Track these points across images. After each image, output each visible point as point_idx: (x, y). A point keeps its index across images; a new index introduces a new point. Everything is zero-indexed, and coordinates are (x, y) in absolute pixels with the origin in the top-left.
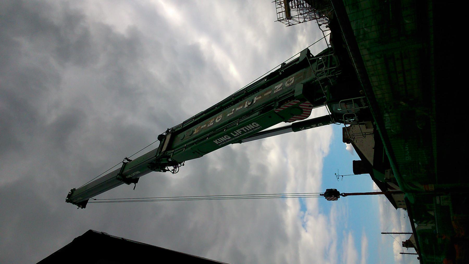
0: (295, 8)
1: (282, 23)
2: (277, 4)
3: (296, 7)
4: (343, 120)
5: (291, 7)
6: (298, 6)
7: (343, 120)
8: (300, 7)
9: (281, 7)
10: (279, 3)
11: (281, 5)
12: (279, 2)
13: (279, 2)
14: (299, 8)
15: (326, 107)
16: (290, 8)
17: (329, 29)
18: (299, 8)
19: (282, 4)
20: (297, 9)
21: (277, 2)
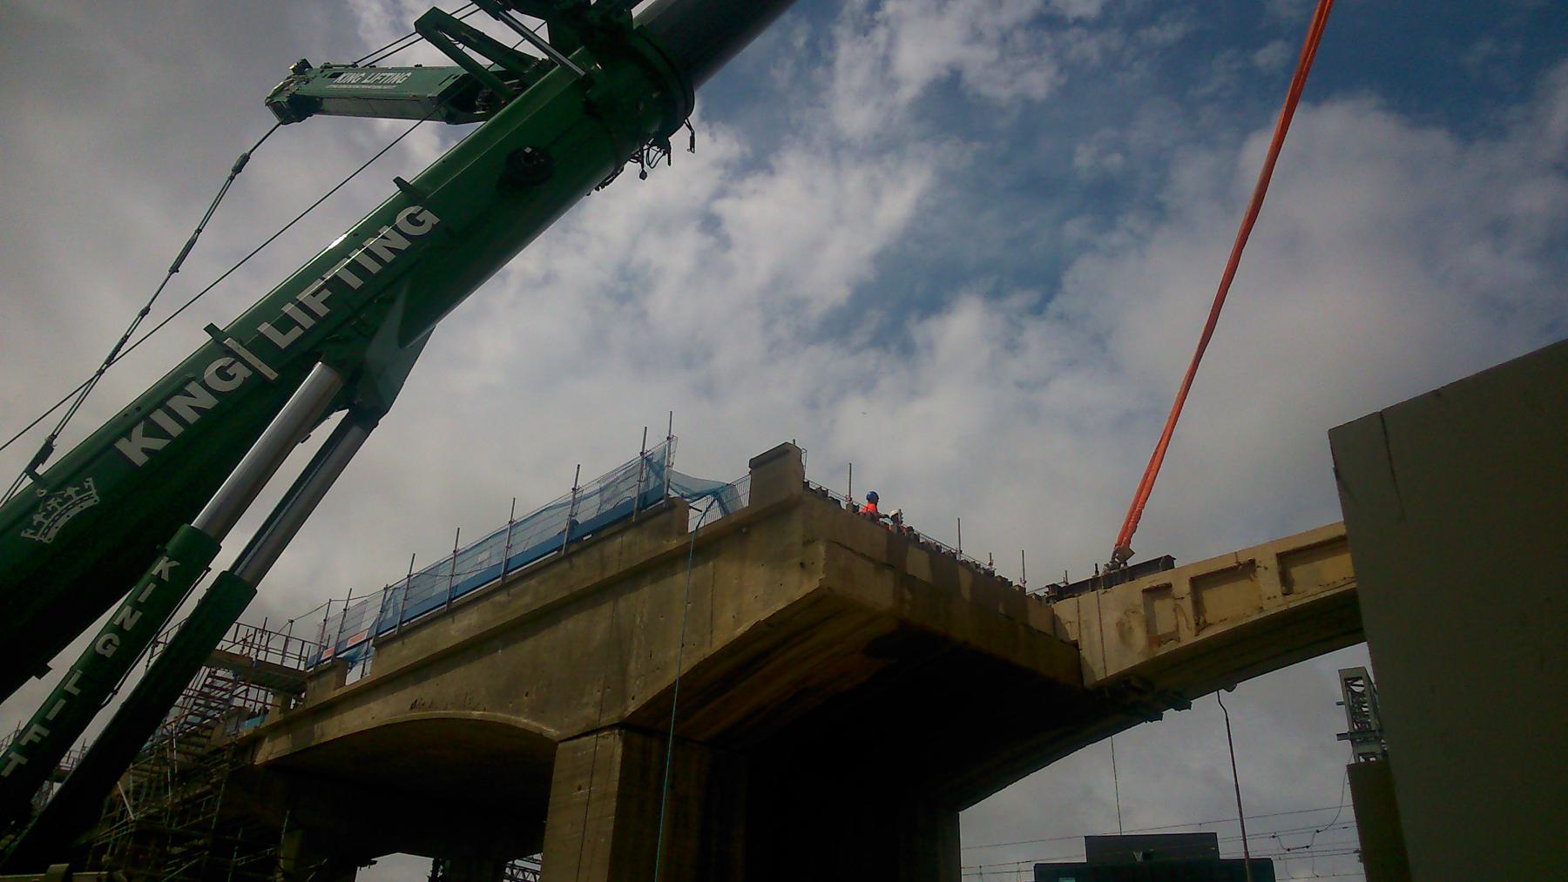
0: (204, 685)
1: (9, 736)
2: (252, 631)
3: (206, 690)
4: (235, 856)
5: (215, 672)
6: (207, 696)
7: (235, 856)
8: (199, 701)
9: (234, 642)
10: (250, 640)
11: (242, 643)
12: (253, 640)
13: (253, 640)
14: (197, 698)
15: (496, 578)
16: (213, 669)
17: (478, 8)
18: (197, 698)
19: (243, 648)
20: (189, 707)
21: (258, 635)
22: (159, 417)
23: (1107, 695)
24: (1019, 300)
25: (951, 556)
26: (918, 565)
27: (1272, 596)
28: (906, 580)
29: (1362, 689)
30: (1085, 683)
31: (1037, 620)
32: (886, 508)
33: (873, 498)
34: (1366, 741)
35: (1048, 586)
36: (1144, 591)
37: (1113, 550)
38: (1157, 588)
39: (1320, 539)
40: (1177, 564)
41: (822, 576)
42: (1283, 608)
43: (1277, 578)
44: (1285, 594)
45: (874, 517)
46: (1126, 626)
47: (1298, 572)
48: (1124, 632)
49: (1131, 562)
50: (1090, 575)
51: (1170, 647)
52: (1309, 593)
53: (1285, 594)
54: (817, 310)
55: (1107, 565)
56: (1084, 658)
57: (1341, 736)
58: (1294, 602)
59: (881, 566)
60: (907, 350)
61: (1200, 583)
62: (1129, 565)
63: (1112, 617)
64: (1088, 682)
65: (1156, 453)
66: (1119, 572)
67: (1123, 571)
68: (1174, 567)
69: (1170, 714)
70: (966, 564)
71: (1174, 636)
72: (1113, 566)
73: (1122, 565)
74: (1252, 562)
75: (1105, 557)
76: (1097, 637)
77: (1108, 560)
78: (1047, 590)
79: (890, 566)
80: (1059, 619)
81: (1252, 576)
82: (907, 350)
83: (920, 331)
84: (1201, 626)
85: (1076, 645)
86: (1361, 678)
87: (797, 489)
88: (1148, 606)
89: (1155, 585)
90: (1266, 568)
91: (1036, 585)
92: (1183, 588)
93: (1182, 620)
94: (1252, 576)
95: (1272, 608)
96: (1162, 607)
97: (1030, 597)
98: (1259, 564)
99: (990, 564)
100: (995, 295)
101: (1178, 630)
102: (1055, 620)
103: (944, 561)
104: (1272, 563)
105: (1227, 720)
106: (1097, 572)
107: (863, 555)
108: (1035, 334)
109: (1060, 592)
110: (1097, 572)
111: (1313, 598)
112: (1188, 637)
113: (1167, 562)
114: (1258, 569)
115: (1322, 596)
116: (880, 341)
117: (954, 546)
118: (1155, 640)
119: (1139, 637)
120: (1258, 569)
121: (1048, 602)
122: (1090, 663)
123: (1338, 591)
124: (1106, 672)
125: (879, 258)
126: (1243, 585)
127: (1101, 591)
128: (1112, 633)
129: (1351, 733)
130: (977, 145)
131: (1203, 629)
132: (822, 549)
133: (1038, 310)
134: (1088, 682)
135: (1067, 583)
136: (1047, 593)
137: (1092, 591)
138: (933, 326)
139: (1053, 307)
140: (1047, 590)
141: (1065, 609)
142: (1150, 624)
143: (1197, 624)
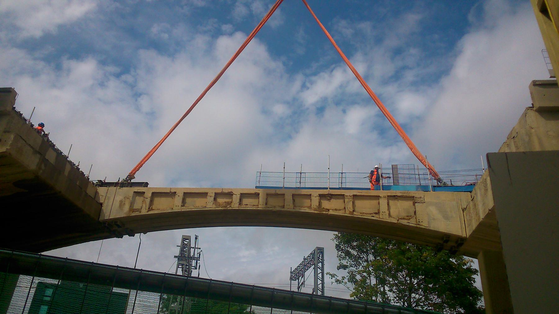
22: (425, 162)
23: (106, 225)
24: (111, 69)
25: (66, 158)
26: (51, 157)
27: (177, 206)
28: (44, 160)
29: (187, 243)
30: (100, 219)
31: (90, 191)
32: (46, 130)
33: (42, 125)
34: (182, 260)
35: (98, 180)
36: (134, 192)
37: (128, 175)
38: (139, 192)
39: (191, 191)
40: (149, 186)
41: (8, 148)
42: (180, 210)
43: (181, 200)
44: (182, 206)
45: (39, 132)
46: (123, 203)
47: (189, 200)
48: (122, 204)
49: (133, 181)
50: (116, 181)
51: (137, 214)
52: (190, 208)
53: (182, 206)
54: (24, 35)
55: (124, 179)
56: (103, 210)
57: (175, 257)
58: (184, 209)
59: (36, 152)
60: (58, 68)
61: (156, 194)
62: (132, 182)
63: (119, 198)
64: (101, 219)
65: (156, 146)
66: (127, 183)
67: (129, 183)
68: (147, 187)
69: (126, 237)
70: (70, 162)
71: (139, 210)
72: (126, 180)
73: (129, 181)
74: (175, 192)
75: (123, 177)
76: (111, 204)
77: (125, 178)
78: (97, 181)
79: (40, 153)
80: (98, 193)
81: (173, 197)
82: (58, 68)
83: (66, 63)
84: (150, 209)
85: (101, 204)
86: (188, 239)
87: (9, 109)
88: (134, 198)
89: (139, 191)
90: (179, 196)
91: (94, 178)
92: (149, 195)
93: (144, 206)
94: (173, 197)
95: (176, 209)
96: (139, 199)
97: (90, 182)
98: (177, 194)
99: (78, 165)
100: (103, 63)
101: (141, 209)
102: (97, 193)
103: (62, 158)
104: (181, 195)
105: (140, 243)
106: (119, 181)
107: (30, 145)
108: (113, 83)
109: (102, 184)
110: (119, 181)
111: (190, 210)
112: (144, 212)
113: (146, 184)
114: (176, 196)
115: (193, 210)
116: (48, 60)
117: (67, 154)
118: (132, 210)
119: (127, 208)
120: (176, 196)
121: (96, 186)
122: (104, 212)
123: (199, 209)
124: (109, 217)
125: (61, 27)
126: (170, 199)
127: (118, 188)
128: (117, 204)
129: (179, 256)
130: (118, 4)
131: (151, 210)
132: (12, 137)
133: (118, 76)
134: (101, 219)
135: (105, 181)
136: (97, 183)
137: (114, 187)
138: (73, 64)
139: (124, 77)
140: (97, 181)
141: (102, 190)
142: (132, 204)
143: (149, 208)
